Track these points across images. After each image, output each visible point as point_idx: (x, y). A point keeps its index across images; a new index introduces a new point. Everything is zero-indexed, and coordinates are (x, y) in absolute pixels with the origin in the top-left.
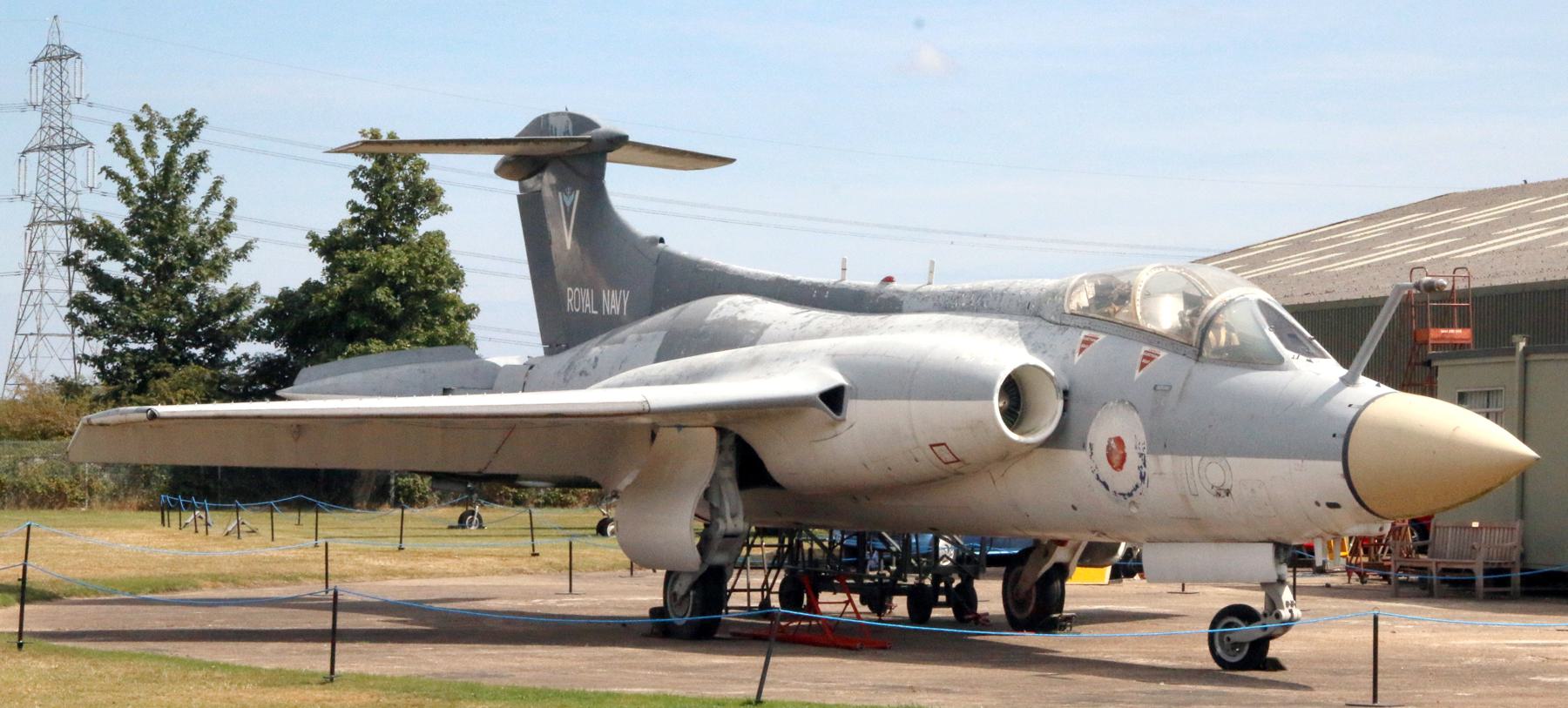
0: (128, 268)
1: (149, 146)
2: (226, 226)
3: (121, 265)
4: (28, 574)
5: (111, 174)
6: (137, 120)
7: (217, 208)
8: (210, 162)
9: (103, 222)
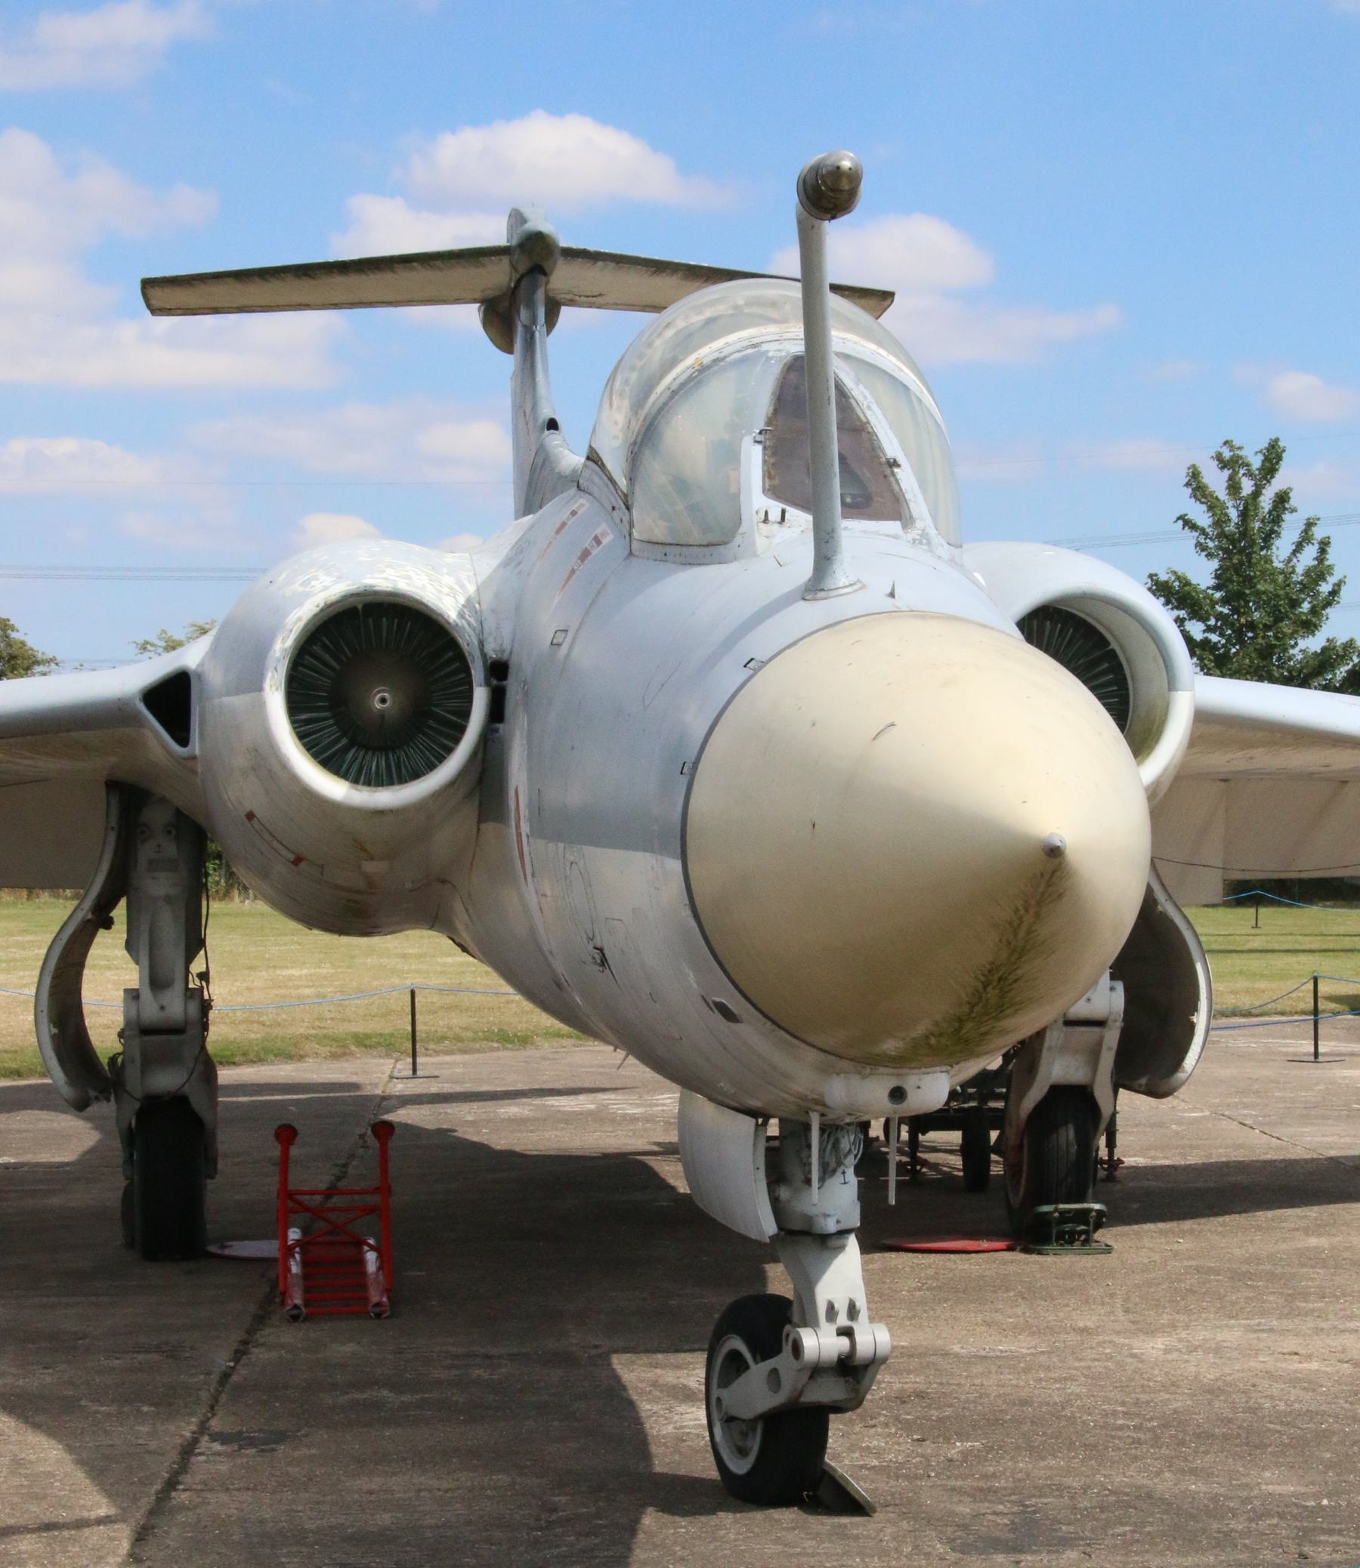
0: (1209, 629)
1: (1234, 487)
2: (1318, 573)
3: (1201, 626)
4: (418, 1028)
5: (1188, 524)
6: (1219, 457)
7: (1310, 553)
8: (1293, 502)
9: (1178, 578)
